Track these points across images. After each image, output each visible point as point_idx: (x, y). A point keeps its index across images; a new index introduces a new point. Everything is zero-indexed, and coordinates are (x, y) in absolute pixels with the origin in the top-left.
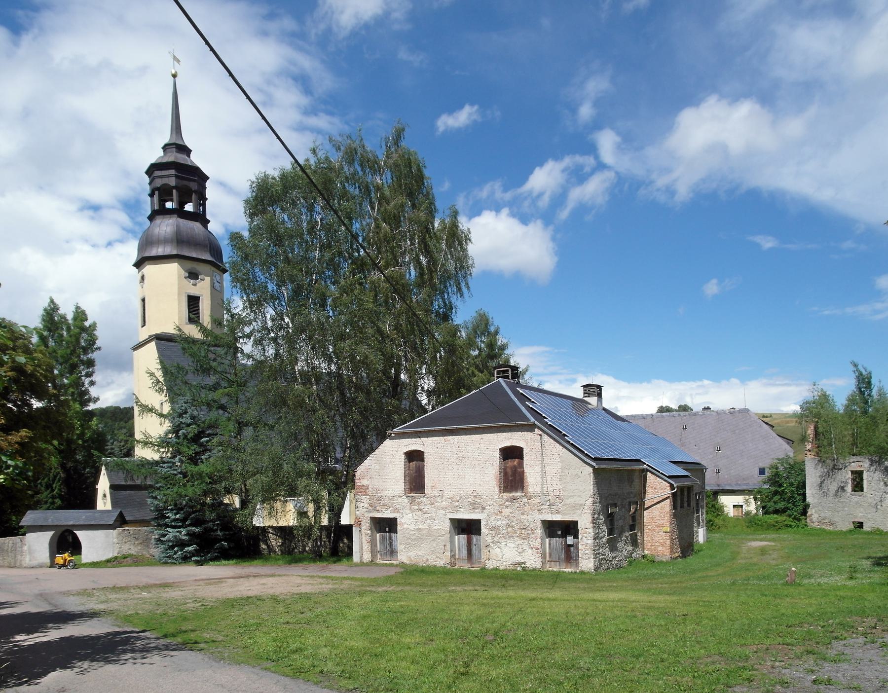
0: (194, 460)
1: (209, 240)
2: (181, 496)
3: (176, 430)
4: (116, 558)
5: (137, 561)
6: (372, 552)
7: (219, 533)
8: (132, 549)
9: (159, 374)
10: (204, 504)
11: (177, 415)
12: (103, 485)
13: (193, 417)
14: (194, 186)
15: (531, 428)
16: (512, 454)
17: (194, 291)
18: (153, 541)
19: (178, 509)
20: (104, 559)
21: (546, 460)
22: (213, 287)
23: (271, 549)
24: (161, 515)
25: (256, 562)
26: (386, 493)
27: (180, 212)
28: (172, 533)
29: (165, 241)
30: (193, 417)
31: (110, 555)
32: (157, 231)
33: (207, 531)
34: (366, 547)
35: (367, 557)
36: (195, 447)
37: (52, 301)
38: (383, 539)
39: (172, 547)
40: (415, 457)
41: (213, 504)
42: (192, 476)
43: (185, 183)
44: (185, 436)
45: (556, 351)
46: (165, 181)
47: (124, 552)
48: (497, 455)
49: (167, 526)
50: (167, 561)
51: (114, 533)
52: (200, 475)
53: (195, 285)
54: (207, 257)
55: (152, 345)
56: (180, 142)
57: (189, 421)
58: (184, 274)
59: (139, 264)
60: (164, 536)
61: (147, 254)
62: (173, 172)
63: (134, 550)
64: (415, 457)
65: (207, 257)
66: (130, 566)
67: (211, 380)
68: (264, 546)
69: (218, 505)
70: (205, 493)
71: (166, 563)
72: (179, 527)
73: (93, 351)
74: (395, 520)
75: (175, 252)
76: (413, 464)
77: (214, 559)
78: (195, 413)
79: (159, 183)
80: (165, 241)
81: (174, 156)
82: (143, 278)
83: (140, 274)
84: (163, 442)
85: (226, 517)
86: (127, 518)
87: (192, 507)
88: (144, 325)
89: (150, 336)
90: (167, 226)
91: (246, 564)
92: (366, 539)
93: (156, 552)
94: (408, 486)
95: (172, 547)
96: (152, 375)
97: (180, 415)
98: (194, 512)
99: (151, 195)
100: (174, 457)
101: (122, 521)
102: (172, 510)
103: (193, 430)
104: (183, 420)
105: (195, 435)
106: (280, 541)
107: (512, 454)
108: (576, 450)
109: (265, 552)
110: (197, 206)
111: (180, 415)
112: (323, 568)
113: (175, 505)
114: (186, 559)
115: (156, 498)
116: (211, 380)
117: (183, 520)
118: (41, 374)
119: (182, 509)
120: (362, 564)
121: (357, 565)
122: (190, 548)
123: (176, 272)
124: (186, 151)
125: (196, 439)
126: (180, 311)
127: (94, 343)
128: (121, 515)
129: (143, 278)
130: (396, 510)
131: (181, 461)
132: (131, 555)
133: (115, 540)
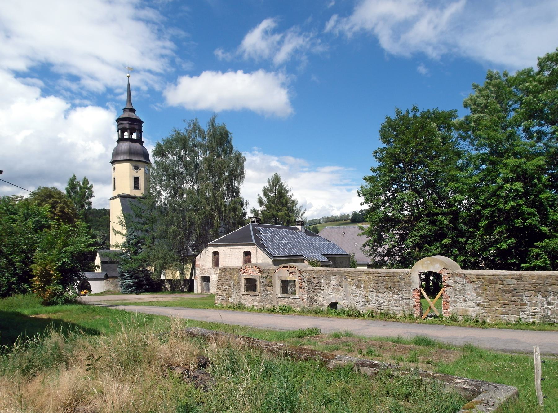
0: (135, 253)
1: (143, 151)
2: (130, 267)
3: (128, 242)
4: (105, 292)
5: (113, 293)
6: (201, 289)
7: (145, 282)
8: (111, 288)
9: (122, 218)
10: (139, 271)
11: (129, 235)
12: (98, 261)
13: (135, 236)
14: (137, 127)
15: (253, 245)
16: (247, 254)
17: (136, 175)
18: (119, 285)
19: (129, 272)
20: (100, 292)
21: (258, 256)
22: (145, 172)
23: (166, 289)
24: (122, 275)
25: (159, 293)
26: (206, 267)
27: (130, 140)
28: (127, 282)
29: (124, 153)
30: (135, 236)
31: (102, 291)
32: (120, 148)
33: (140, 281)
34: (199, 287)
35: (199, 291)
36: (136, 248)
37: (74, 176)
38: (206, 284)
39: (127, 287)
40: (216, 254)
41: (142, 271)
42: (134, 260)
43: (133, 126)
44: (132, 243)
45: (346, 169)
46: (124, 125)
47: (108, 290)
48: (243, 254)
49: (125, 279)
50: (125, 293)
51: (104, 282)
52: (137, 260)
53: (137, 172)
54: (142, 159)
55: (118, 199)
56: (131, 107)
57: (133, 237)
58: (132, 167)
59: (113, 162)
60: (124, 283)
61: (116, 159)
62: (127, 122)
63: (111, 289)
64: (216, 254)
65: (142, 159)
66: (110, 295)
67: (142, 220)
68: (163, 288)
69: (145, 271)
70: (139, 266)
71: (124, 294)
72: (129, 280)
73: (91, 198)
74: (209, 277)
75: (128, 158)
76: (216, 256)
77: (143, 292)
78: (136, 234)
79: (121, 126)
80: (124, 153)
81: (127, 115)
82: (114, 168)
83: (113, 167)
84: (124, 245)
85: (147, 275)
86: (109, 276)
87: (134, 272)
88: (115, 189)
89: (118, 195)
90: (125, 146)
91: (155, 294)
92: (199, 284)
93: (120, 289)
94: (214, 265)
95: (127, 287)
96: (119, 218)
97: (130, 235)
98: (135, 274)
99: (118, 131)
100: (127, 252)
101: (107, 277)
102: (127, 273)
103: (135, 241)
104: (131, 237)
105: (136, 243)
106: (517, 225)
107: (247, 254)
108: (268, 253)
109: (164, 290)
110: (138, 136)
111: (130, 235)
112: (182, 295)
113: (128, 271)
114: (132, 292)
115: (120, 268)
116: (142, 220)
117: (131, 277)
118: (71, 213)
119: (130, 272)
120: (197, 294)
121: (195, 294)
122: (134, 288)
123: (129, 167)
124: (133, 111)
125: (136, 245)
126: (130, 185)
127: (92, 194)
128: (106, 275)
129: (114, 168)
130: (210, 274)
131: (130, 253)
132: (110, 291)
133: (104, 285)
